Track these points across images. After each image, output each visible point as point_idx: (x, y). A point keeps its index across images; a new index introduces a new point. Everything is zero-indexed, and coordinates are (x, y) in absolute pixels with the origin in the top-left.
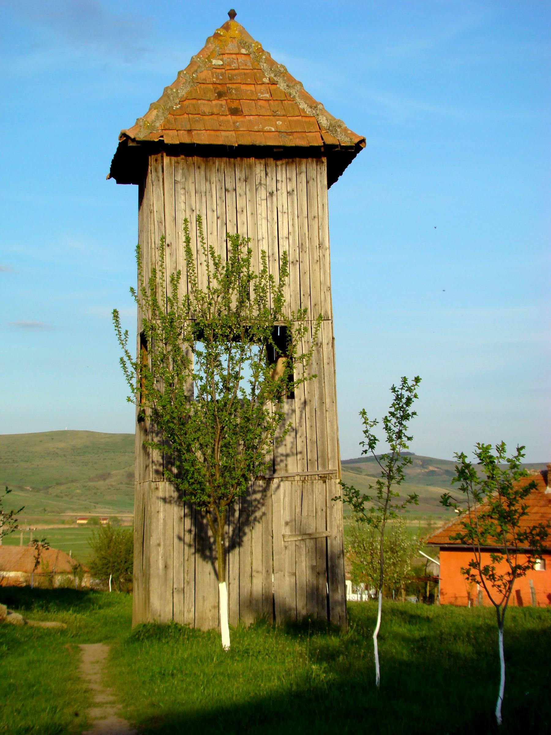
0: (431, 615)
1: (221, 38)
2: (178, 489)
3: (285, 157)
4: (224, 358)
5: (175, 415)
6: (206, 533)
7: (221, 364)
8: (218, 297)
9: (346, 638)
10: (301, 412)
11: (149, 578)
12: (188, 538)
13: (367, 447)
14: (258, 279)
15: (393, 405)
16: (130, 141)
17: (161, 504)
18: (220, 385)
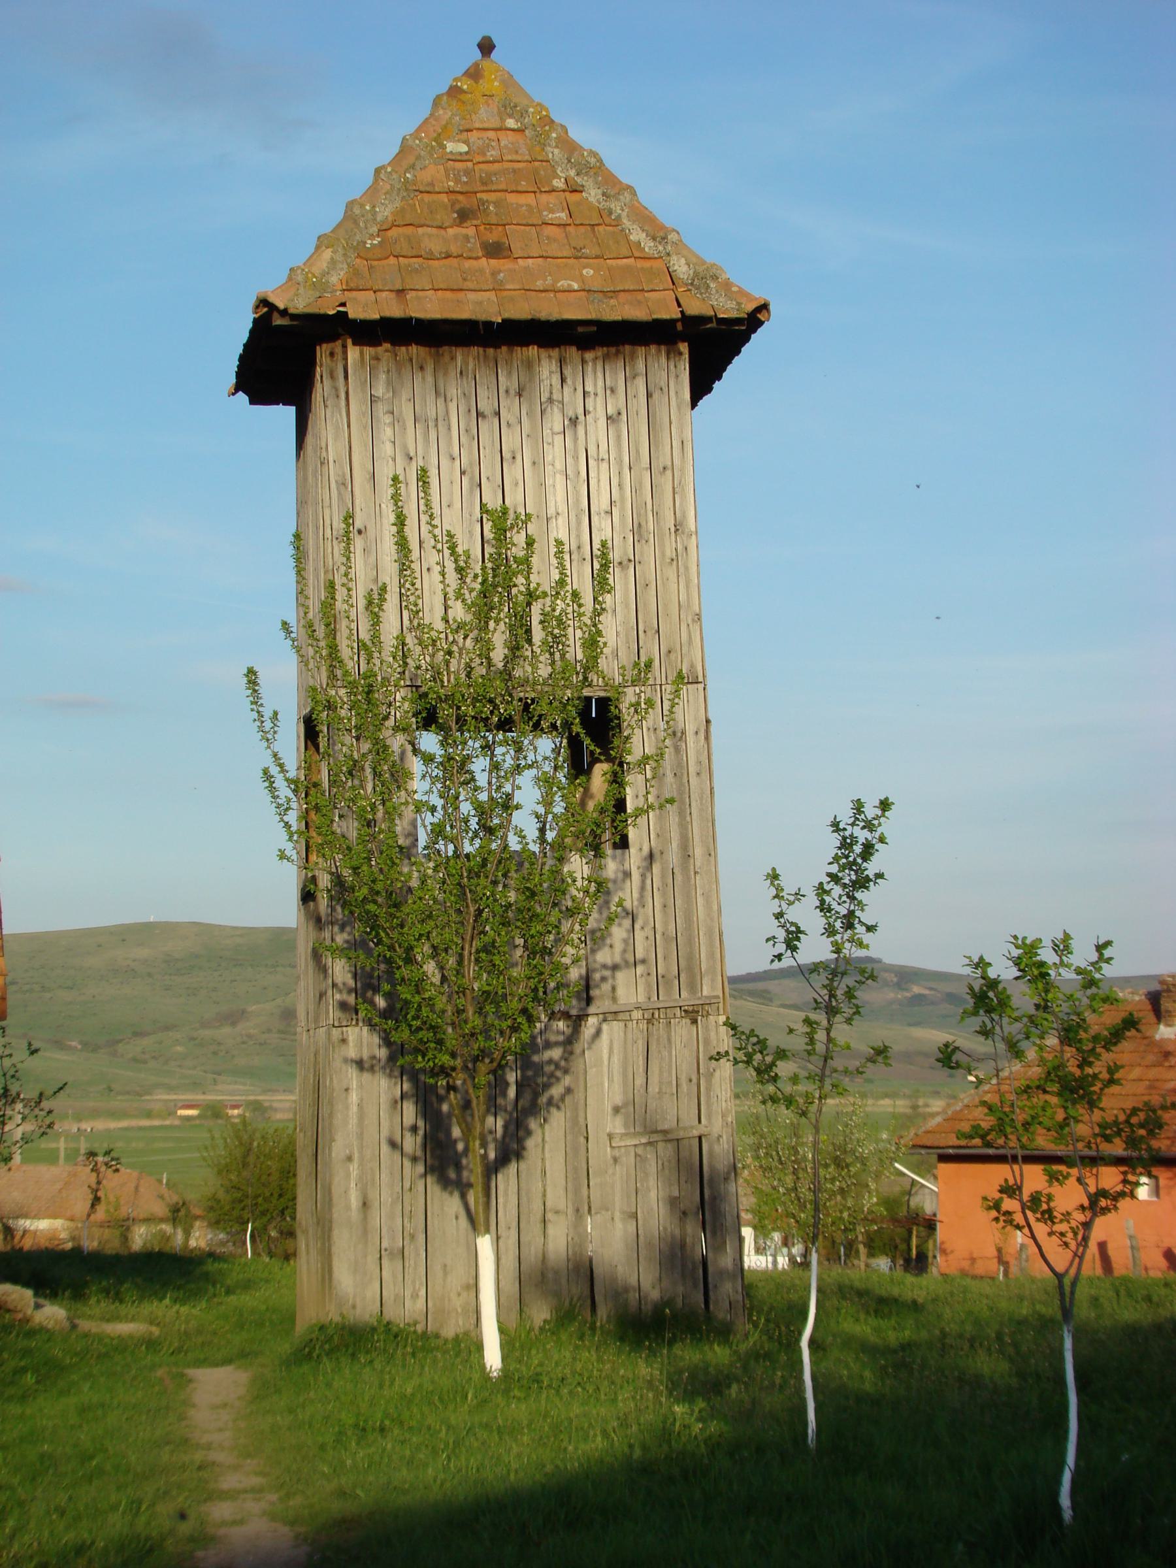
0: (921, 1296)
1: (463, 97)
2: (387, 1042)
3: (603, 344)
4: (480, 766)
5: (379, 886)
6: (448, 1133)
7: (473, 779)
8: (465, 638)
9: (743, 1347)
10: (643, 876)
11: (330, 1229)
12: (411, 1144)
13: (781, 948)
14: (548, 600)
15: (836, 859)
16: (275, 315)
17: (352, 1072)
18: (473, 823)
